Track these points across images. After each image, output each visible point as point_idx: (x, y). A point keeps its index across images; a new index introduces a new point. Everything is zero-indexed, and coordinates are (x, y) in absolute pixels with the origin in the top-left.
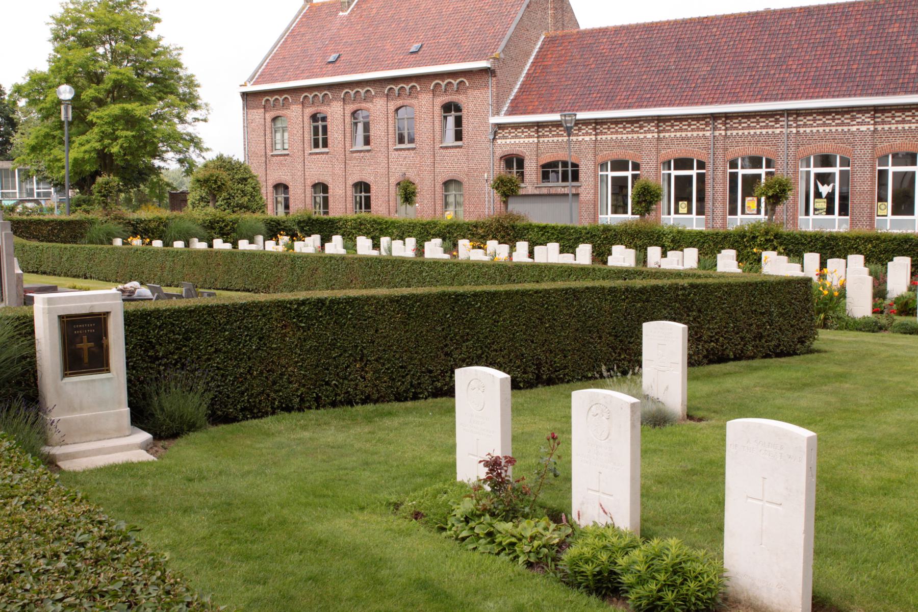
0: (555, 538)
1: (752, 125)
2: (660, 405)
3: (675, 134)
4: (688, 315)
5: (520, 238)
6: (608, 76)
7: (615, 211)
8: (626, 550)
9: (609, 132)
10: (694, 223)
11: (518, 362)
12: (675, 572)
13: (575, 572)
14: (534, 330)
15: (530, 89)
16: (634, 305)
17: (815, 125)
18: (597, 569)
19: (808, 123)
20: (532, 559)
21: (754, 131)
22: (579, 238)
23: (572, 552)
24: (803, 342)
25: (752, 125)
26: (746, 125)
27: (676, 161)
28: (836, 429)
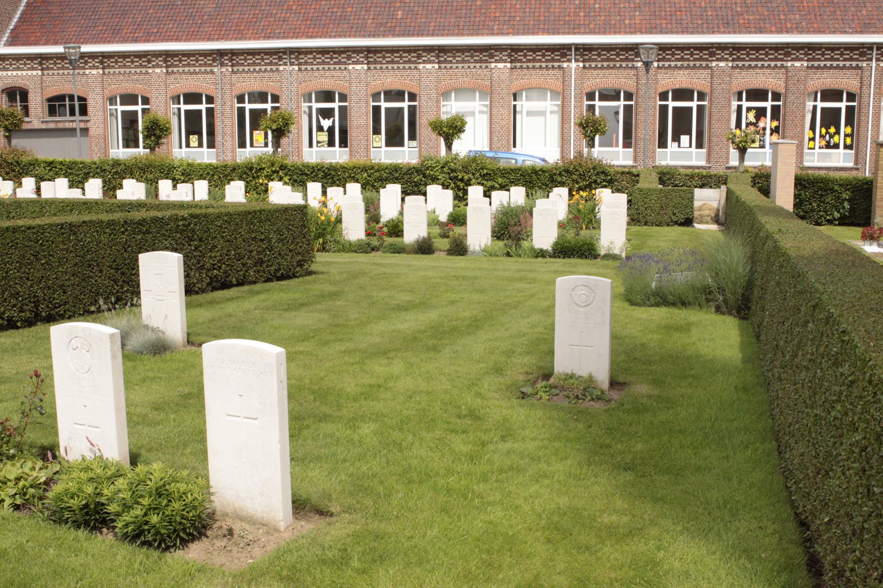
0: (41, 477)
1: (257, 61)
2: (160, 334)
3: (183, 69)
4: (190, 245)
5: (26, 174)
6: (114, 9)
7: (127, 145)
8: (112, 479)
9: (117, 66)
10: (206, 156)
11: (13, 301)
12: (160, 495)
13: (62, 508)
14: (29, 267)
15: (30, 20)
16: (134, 238)
17: (315, 63)
18: (84, 502)
19: (309, 61)
20: (18, 502)
21: (259, 67)
22: (88, 173)
23: (57, 489)
24: (301, 266)
25: (257, 61)
26: (251, 61)
27: (823, 92)
28: (326, 343)
